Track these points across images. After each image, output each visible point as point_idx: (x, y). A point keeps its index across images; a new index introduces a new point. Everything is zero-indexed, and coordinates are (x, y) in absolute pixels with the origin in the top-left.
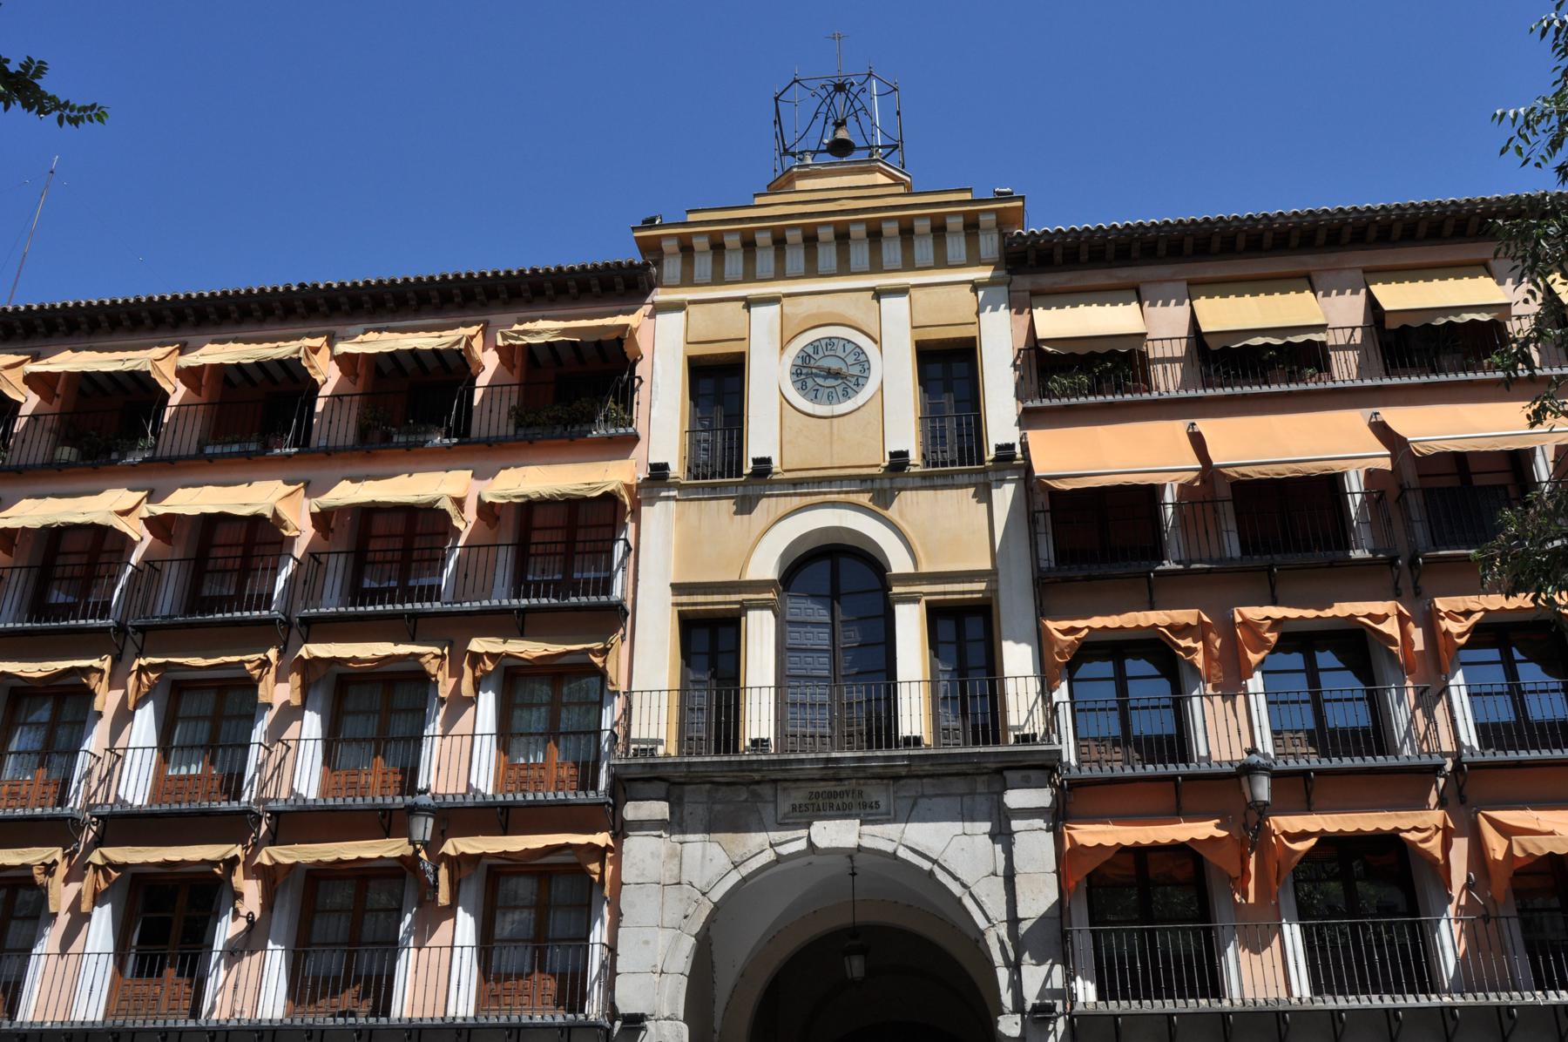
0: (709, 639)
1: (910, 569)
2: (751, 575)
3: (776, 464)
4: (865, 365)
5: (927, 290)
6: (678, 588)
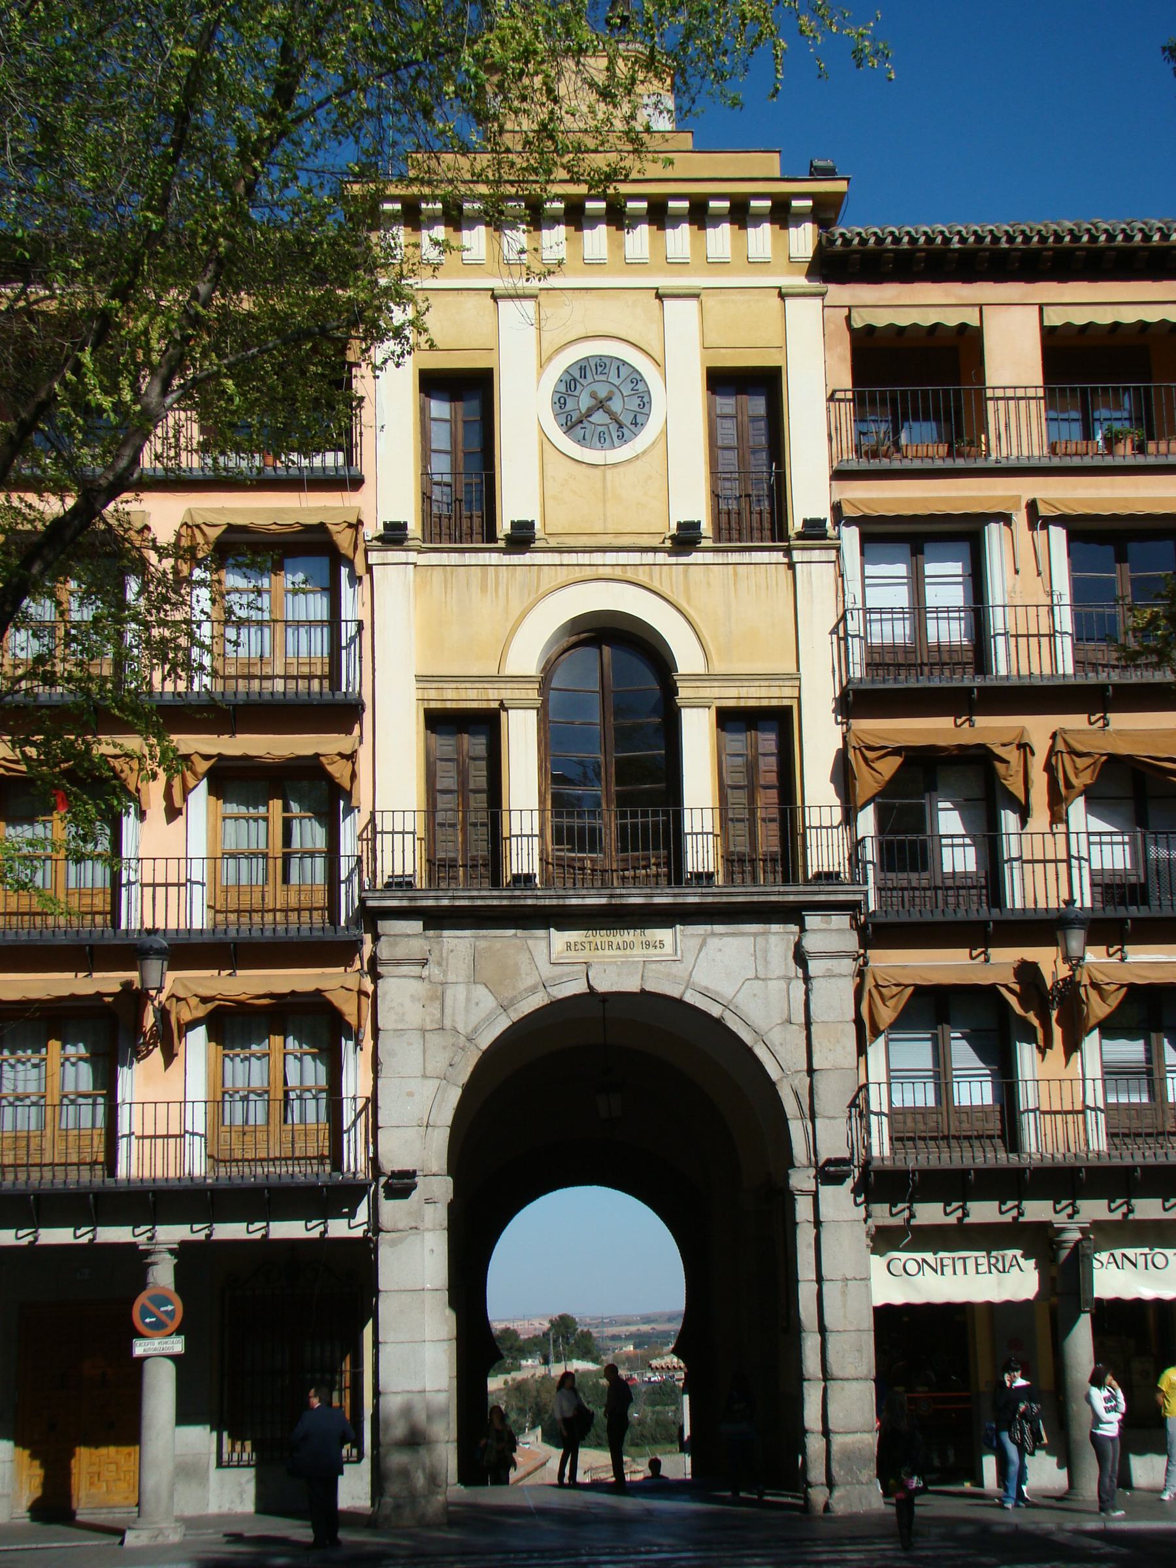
0: (462, 729)
1: (700, 669)
2: (510, 669)
3: (538, 526)
4: (645, 402)
5: (938, 309)
6: (420, 678)
